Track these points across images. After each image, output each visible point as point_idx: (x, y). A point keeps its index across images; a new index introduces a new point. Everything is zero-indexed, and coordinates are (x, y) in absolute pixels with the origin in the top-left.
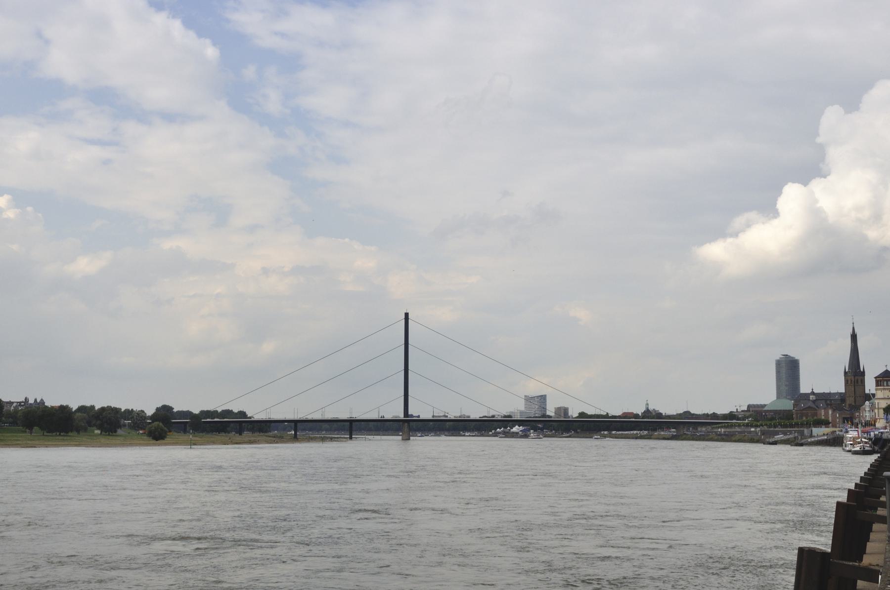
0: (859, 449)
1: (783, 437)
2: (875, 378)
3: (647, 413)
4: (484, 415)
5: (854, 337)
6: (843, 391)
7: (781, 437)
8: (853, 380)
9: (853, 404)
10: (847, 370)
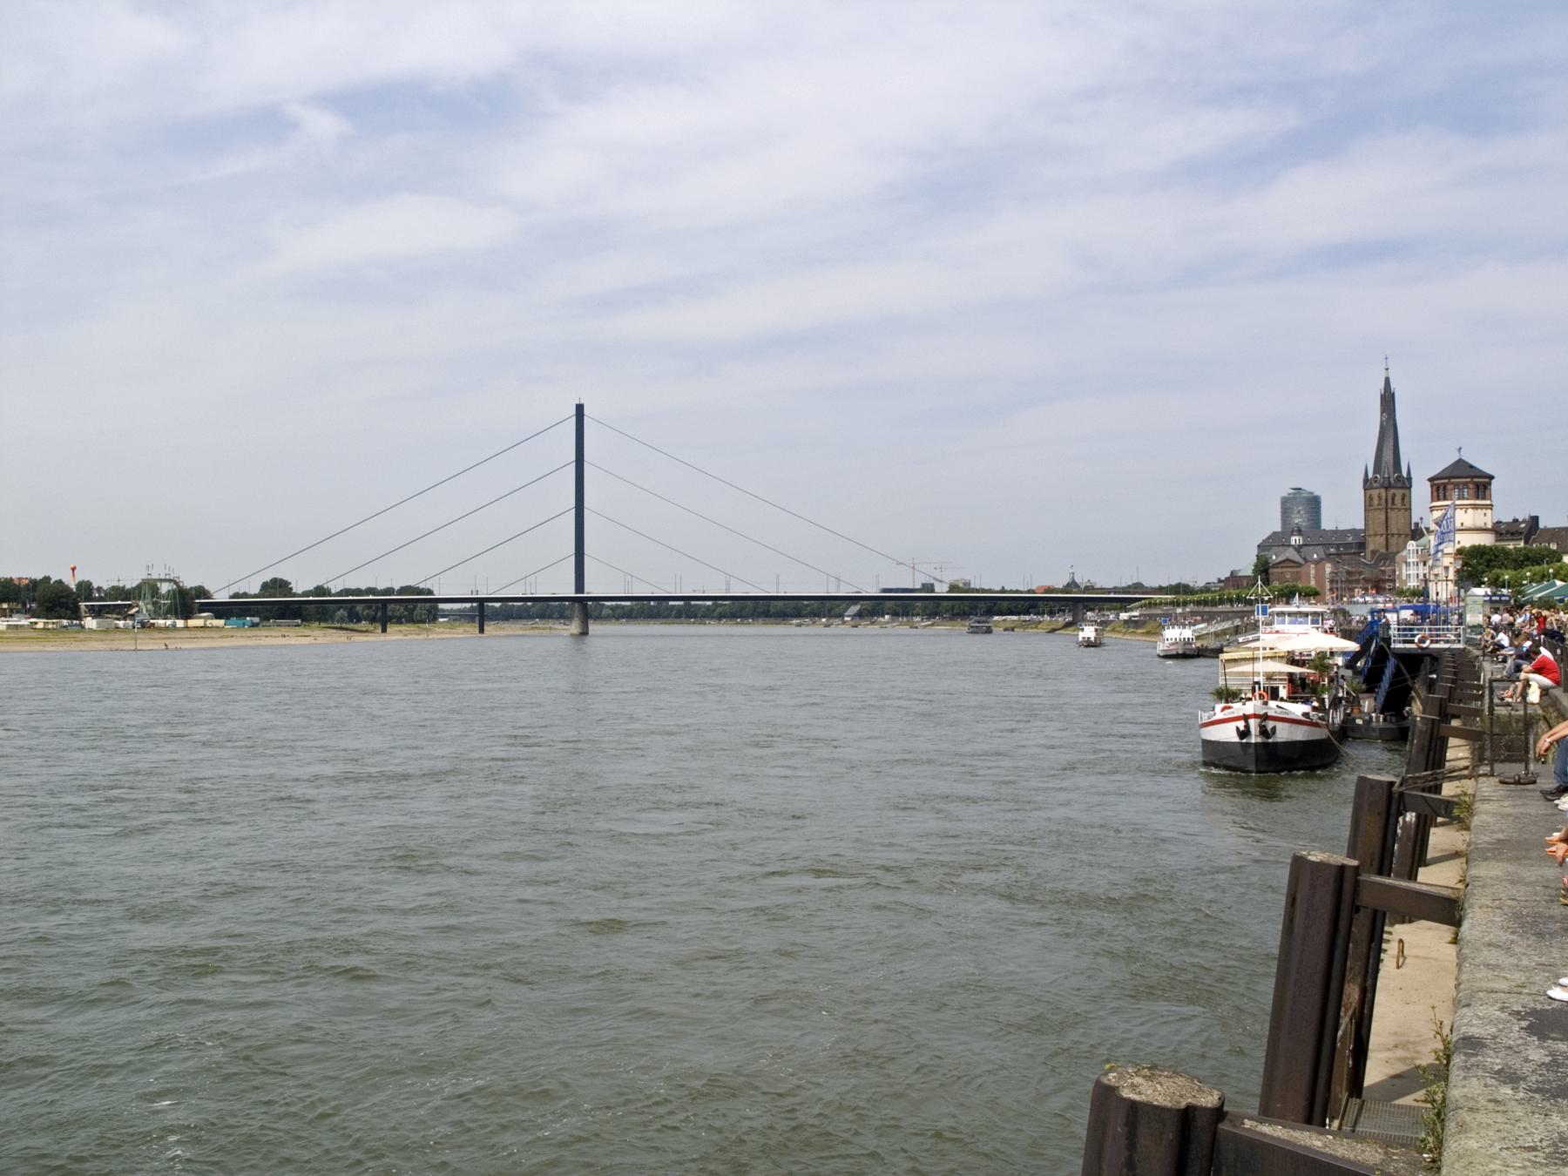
0: (1236, 739)
1: (1206, 628)
3: (1072, 585)
5: (1388, 401)
6: (1360, 525)
7: (1202, 629)
8: (1384, 497)
9: (1383, 550)
10: (1370, 475)
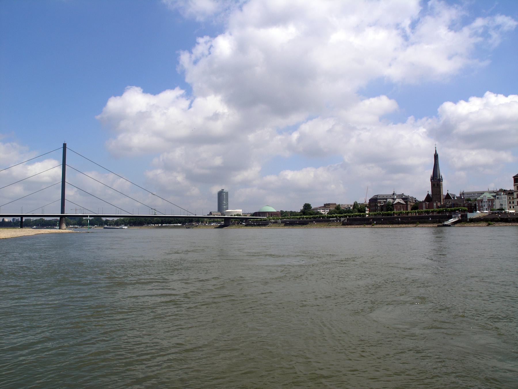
2: (513, 177)
4: (374, 195)
5: (436, 156)
7: (453, 220)
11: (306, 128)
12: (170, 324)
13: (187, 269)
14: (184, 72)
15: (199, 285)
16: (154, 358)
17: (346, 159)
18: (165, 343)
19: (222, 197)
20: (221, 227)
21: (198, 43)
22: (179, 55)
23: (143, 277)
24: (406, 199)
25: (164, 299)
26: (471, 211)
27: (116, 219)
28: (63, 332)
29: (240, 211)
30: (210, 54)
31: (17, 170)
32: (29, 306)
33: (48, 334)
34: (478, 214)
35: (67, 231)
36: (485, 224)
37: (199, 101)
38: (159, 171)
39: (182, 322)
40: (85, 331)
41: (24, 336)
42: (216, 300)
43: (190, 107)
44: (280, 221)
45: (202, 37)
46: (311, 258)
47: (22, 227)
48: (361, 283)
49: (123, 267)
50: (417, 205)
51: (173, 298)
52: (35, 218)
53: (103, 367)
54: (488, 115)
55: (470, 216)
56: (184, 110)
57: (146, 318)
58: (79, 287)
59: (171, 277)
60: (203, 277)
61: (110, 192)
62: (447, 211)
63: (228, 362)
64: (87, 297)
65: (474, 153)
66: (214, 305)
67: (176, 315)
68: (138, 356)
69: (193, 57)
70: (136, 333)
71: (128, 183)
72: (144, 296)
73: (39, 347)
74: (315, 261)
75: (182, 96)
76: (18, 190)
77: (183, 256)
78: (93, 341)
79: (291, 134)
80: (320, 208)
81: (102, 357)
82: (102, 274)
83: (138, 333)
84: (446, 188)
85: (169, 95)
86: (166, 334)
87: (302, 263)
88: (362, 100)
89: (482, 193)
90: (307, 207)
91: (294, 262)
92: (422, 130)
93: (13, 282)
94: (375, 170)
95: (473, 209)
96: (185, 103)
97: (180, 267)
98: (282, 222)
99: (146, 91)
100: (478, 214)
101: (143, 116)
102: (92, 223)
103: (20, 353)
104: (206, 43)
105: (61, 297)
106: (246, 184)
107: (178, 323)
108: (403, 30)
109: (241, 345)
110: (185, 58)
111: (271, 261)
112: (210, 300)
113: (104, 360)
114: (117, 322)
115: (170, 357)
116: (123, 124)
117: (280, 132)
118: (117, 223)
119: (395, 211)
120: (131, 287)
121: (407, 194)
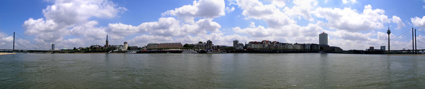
5: (107, 36)
11: (75, 28)
12: (39, 77)
13: (44, 64)
14: (43, 14)
15: (47, 68)
16: (36, 85)
17: (85, 36)
18: (38, 82)
19: (53, 45)
20: (53, 53)
21: (47, 7)
22: (42, 10)
23: (33, 65)
24: (99, 46)
25: (38, 71)
26: (114, 50)
27: (26, 51)
28: (14, 78)
29: (57, 49)
30: (50, 9)
31: (4, 39)
32: (6, 71)
33: (10, 78)
34: (116, 50)
35: (15, 53)
36: (117, 53)
37: (47, 21)
38: (37, 39)
39: (43, 77)
40: (19, 78)
41: (5, 78)
42: (51, 72)
43: (45, 23)
44: (68, 52)
45: (48, 5)
46: (76, 61)
47: (4, 52)
48: (88, 67)
49: (28, 63)
50: (102, 48)
51: (40, 71)
52: (7, 50)
53: (23, 86)
54: (119, 28)
55: (114, 51)
56: (43, 24)
57: (33, 75)
58: (17, 67)
59: (40, 66)
60: (48, 66)
61: (25, 44)
62: (109, 49)
63: (54, 87)
64: (19, 70)
65: (116, 36)
66: (51, 73)
67: (41, 75)
68: (32, 84)
69: (46, 10)
70: (31, 79)
71: (29, 42)
72: (33, 70)
73: (8, 81)
74: (77, 62)
75: (43, 20)
76: (4, 43)
77: (43, 60)
78: (21, 80)
79: (71, 30)
80: (78, 49)
81: (23, 84)
82: (23, 64)
83: (32, 79)
84: (109, 44)
85: (40, 20)
86: (39, 80)
87: (73, 62)
88: (89, 21)
89: (117, 46)
90: (75, 48)
91: (71, 62)
92: (104, 30)
93: (2, 65)
94: (92, 39)
95: (115, 49)
96: (44, 22)
97: (42, 63)
98: (68, 52)
99: (34, 19)
100: (116, 50)
101: (33, 25)
102: (21, 52)
103: (4, 81)
104: (49, 7)
105: (13, 69)
106: (59, 42)
107: (42, 77)
108: (99, 5)
109: (58, 83)
110: (44, 11)
111: (65, 62)
112: (50, 72)
113: (23, 85)
114: (26, 76)
115: (40, 85)
116: (28, 27)
117: (68, 29)
118: (27, 52)
119: (97, 49)
120: (30, 68)
121: (100, 45)
